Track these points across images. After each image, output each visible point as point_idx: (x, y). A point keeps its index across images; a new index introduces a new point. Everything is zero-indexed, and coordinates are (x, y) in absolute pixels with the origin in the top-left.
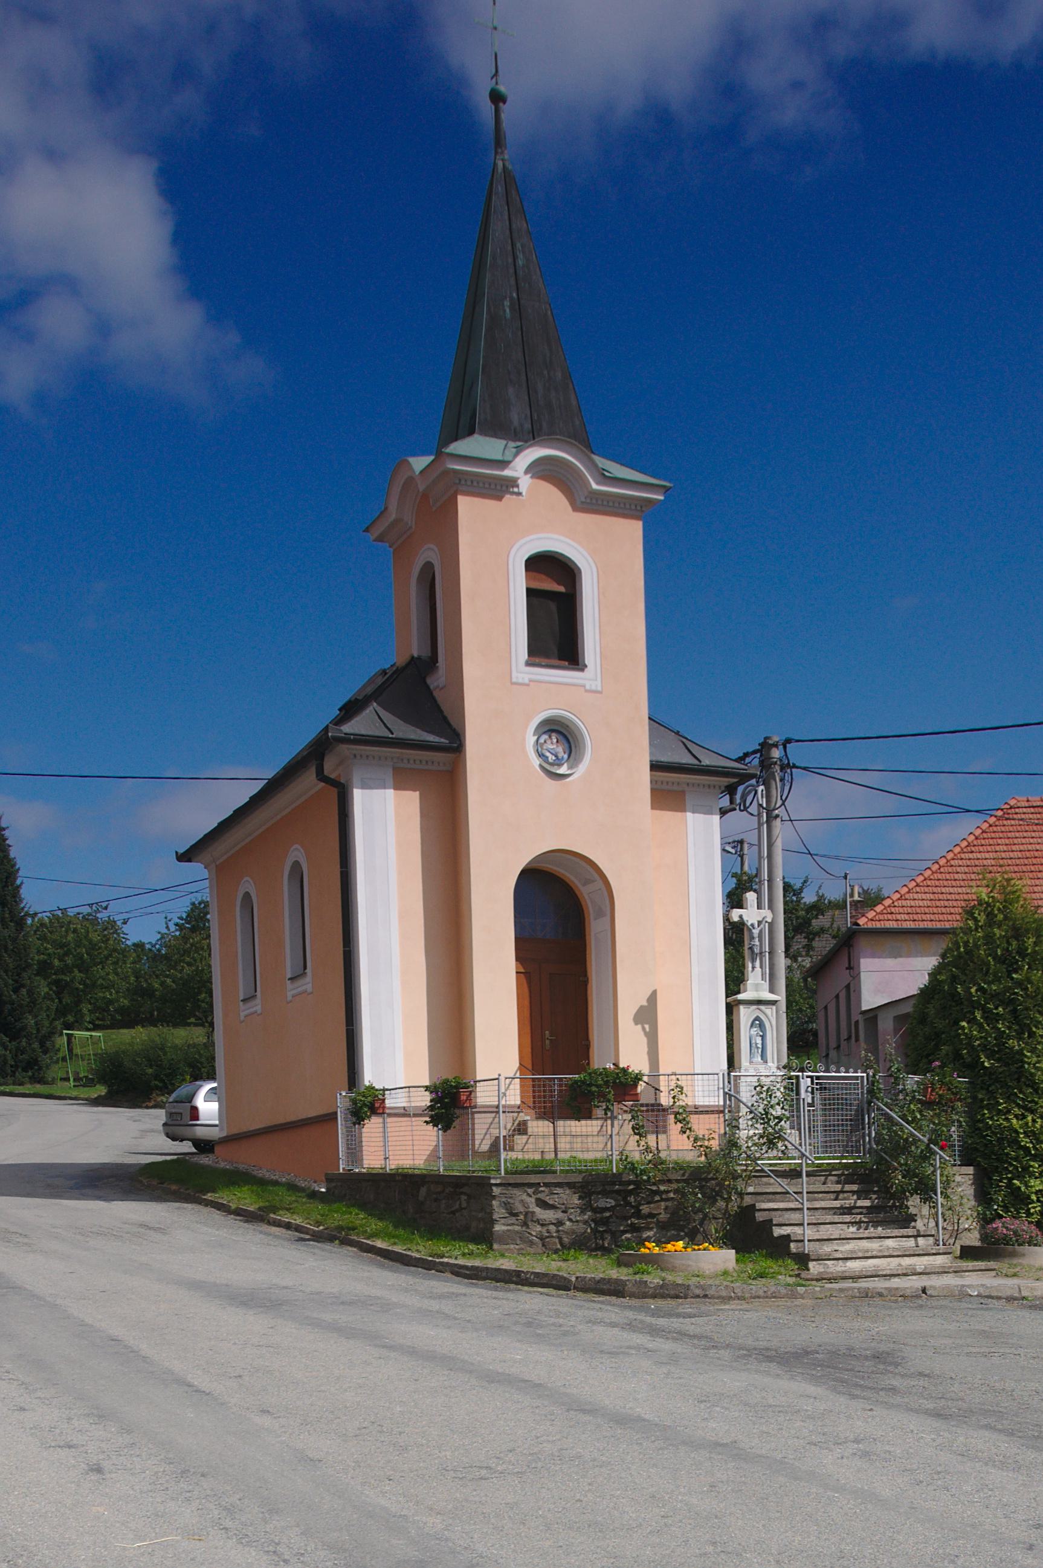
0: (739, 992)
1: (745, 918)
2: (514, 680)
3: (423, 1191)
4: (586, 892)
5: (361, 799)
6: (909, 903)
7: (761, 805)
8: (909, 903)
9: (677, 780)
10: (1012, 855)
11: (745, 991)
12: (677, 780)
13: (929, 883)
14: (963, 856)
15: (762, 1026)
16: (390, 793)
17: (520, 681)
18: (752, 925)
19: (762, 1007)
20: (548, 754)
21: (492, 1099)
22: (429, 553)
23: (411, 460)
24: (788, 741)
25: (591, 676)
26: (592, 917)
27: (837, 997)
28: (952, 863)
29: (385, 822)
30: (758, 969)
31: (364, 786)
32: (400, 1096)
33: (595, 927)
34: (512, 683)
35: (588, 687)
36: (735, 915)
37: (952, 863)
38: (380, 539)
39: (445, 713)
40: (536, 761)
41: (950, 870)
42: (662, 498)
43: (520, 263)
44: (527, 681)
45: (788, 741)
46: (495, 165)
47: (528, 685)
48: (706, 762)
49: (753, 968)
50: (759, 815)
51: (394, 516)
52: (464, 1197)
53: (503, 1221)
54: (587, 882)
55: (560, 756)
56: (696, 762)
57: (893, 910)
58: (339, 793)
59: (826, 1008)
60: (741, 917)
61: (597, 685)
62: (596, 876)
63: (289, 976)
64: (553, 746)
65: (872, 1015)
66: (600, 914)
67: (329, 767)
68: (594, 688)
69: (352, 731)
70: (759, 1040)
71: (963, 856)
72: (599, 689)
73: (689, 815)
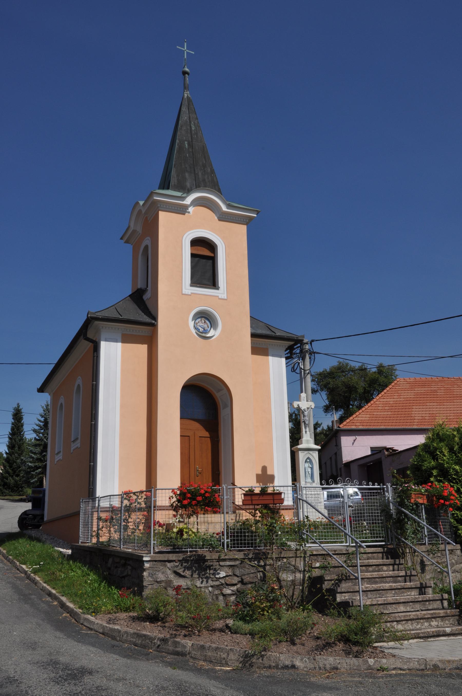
0: (298, 444)
1: (300, 406)
2: (184, 293)
3: (111, 560)
4: (218, 396)
5: (104, 346)
6: (360, 419)
7: (301, 368)
8: (360, 419)
9: (264, 339)
10: (400, 399)
11: (302, 443)
12: (264, 339)
13: (368, 411)
14: (380, 400)
15: (311, 462)
16: (120, 344)
17: (187, 293)
18: (304, 410)
19: (311, 452)
20: (200, 328)
21: (106, 503)
22: (147, 241)
23: (139, 202)
24: (313, 341)
25: (222, 292)
26: (215, 393)
27: (331, 458)
28: (377, 403)
29: (115, 358)
30: (308, 432)
31: (106, 340)
32: (115, 500)
33: (223, 413)
34: (183, 294)
35: (220, 297)
36: (295, 404)
37: (377, 403)
38: (127, 242)
39: (150, 310)
40: (194, 331)
41: (376, 405)
42: (256, 216)
43: (193, 129)
44: (190, 293)
45: (313, 341)
46: (184, 95)
47: (190, 295)
48: (278, 334)
49: (306, 432)
50: (301, 372)
51: (132, 229)
52: (129, 568)
53: (150, 587)
54: (219, 390)
55: (206, 329)
56: (273, 334)
57: (354, 421)
58: (94, 346)
59: (326, 463)
60: (298, 405)
61: (224, 296)
62: (224, 388)
63: (72, 440)
64: (201, 323)
65: (348, 464)
66: (225, 406)
67: (90, 334)
68: (223, 297)
69: (101, 315)
70: (309, 470)
71: (380, 400)
72: (226, 298)
73: (270, 358)
